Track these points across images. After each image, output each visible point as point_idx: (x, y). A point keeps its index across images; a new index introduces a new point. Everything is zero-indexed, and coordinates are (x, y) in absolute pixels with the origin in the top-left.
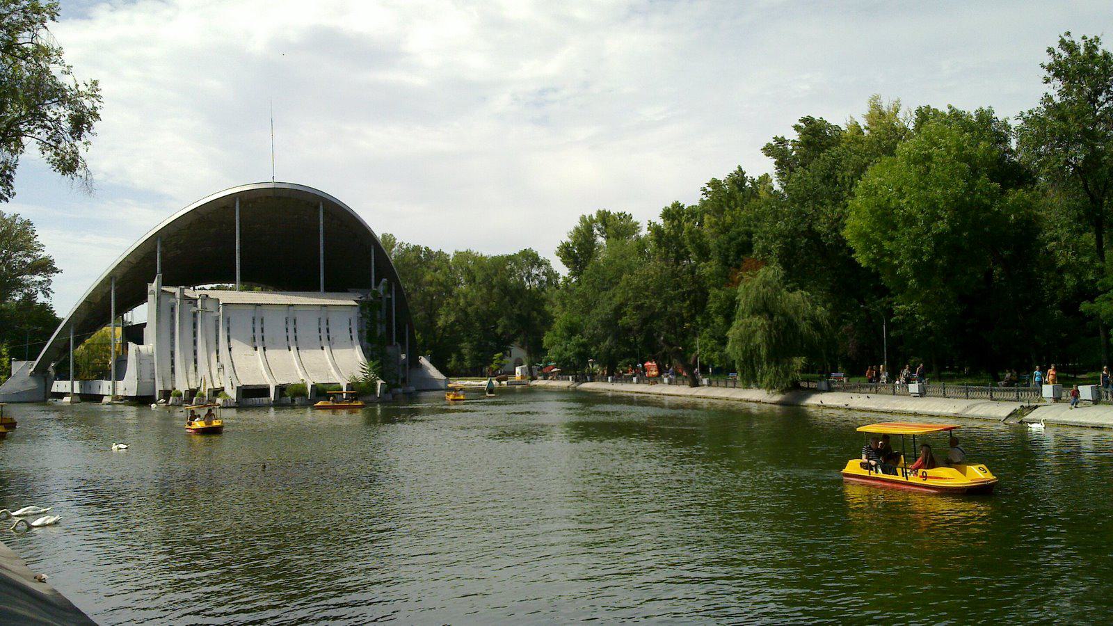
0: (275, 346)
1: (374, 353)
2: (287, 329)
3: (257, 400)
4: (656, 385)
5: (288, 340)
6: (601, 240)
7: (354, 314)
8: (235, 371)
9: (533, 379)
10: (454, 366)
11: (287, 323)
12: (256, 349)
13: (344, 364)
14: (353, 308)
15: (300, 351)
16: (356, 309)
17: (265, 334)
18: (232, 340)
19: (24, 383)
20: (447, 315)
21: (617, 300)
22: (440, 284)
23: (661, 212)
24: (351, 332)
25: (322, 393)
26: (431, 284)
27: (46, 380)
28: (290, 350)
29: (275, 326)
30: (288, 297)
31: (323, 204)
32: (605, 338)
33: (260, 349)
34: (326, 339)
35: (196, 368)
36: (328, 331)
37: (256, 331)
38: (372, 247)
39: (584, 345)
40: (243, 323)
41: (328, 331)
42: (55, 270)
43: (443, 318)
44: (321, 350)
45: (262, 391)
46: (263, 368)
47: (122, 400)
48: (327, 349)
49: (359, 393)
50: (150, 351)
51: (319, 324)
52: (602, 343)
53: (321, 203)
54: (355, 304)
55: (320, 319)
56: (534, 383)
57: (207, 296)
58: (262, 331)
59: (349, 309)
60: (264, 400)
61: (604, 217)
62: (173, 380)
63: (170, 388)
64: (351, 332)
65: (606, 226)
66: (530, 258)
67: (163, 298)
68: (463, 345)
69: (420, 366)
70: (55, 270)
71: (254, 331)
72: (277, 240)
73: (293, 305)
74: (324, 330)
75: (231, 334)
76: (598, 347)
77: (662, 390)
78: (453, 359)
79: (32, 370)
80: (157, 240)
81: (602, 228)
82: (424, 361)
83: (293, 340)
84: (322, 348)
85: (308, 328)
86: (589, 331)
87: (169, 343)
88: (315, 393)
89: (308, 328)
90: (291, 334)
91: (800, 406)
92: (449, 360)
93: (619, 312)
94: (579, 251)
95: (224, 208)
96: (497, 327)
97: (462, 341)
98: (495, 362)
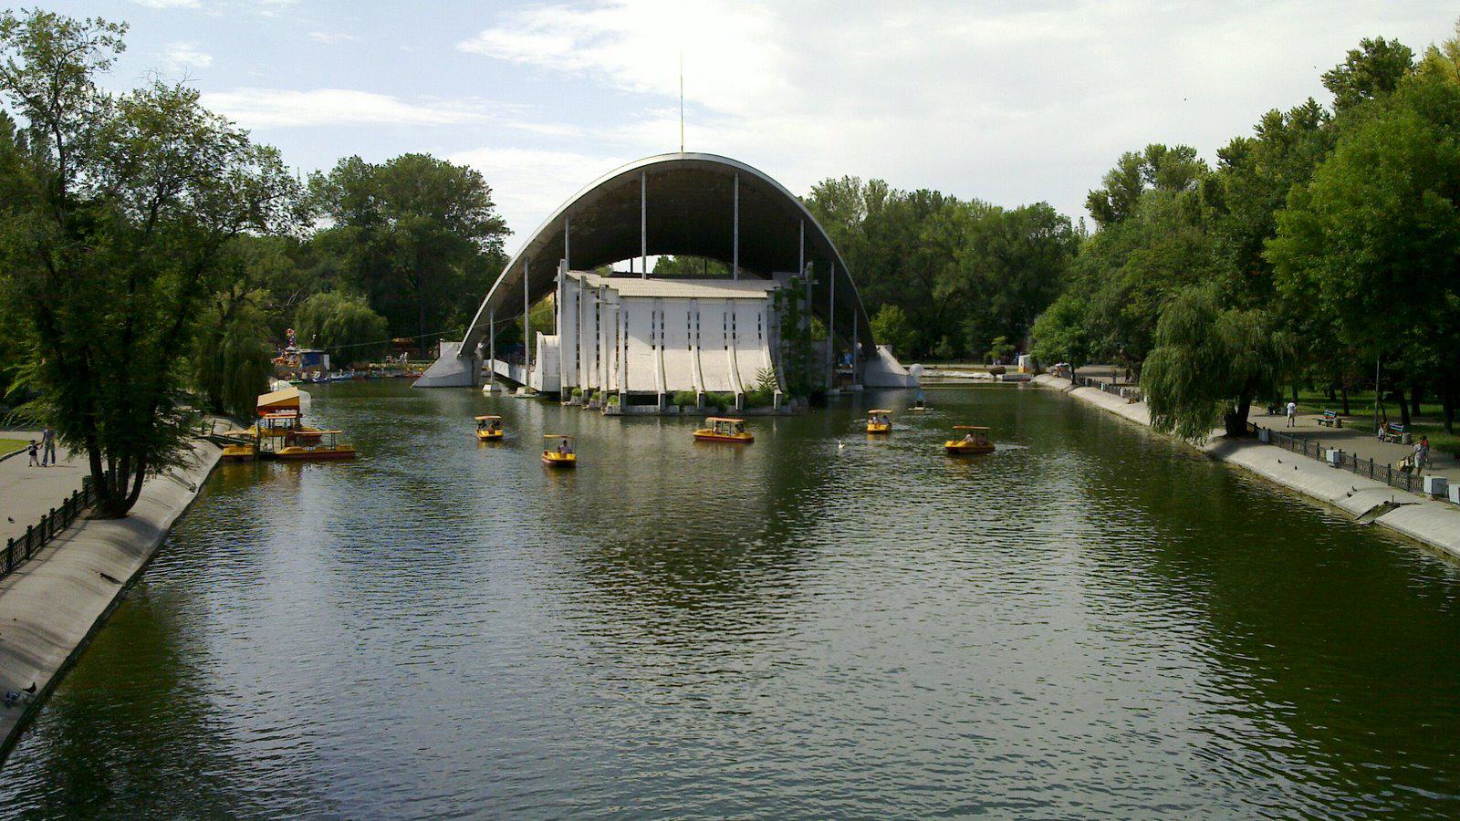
0: (675, 346)
1: (792, 352)
2: (689, 325)
3: (643, 408)
4: (1136, 404)
5: (689, 338)
6: (1149, 186)
7: (762, 308)
8: (626, 374)
9: (1039, 372)
10: (943, 352)
11: (689, 318)
12: (654, 348)
13: (743, 366)
14: (764, 301)
15: (701, 351)
16: (766, 302)
17: (665, 331)
18: (629, 337)
19: (452, 366)
20: (946, 284)
21: (1126, 282)
22: (939, 245)
23: (1085, 200)
24: (760, 329)
25: (714, 404)
26: (928, 244)
27: (473, 363)
28: (690, 349)
29: (676, 322)
30: (695, 286)
31: (739, 176)
32: (1108, 333)
33: (658, 348)
34: (731, 337)
35: (598, 365)
36: (734, 328)
37: (656, 328)
38: (802, 222)
39: (1082, 339)
40: (641, 318)
41: (734, 328)
42: (507, 231)
43: (939, 287)
44: (724, 351)
45: (649, 398)
46: (656, 371)
47: (533, 394)
48: (730, 349)
49: (751, 406)
50: (556, 344)
51: (725, 320)
52: (1105, 337)
53: (737, 175)
54: (765, 295)
55: (725, 314)
56: (1040, 379)
57: (607, 286)
58: (662, 328)
59: (758, 302)
60: (651, 408)
61: (1156, 154)
62: (578, 376)
63: (574, 385)
64: (760, 329)
65: (1158, 167)
66: (1042, 216)
67: (568, 285)
68: (966, 322)
69: (877, 358)
70: (507, 231)
71: (653, 327)
72: (693, 214)
73: (695, 298)
74: (729, 327)
75: (629, 331)
76: (1099, 342)
77: (1132, 413)
78: (943, 343)
79: (459, 352)
80: (565, 217)
81: (1152, 171)
82: (884, 351)
83: (695, 339)
84: (726, 348)
85: (712, 323)
86: (1089, 321)
87: (574, 338)
88: (703, 402)
89: (712, 323)
90: (693, 331)
91: (1222, 461)
92: (937, 343)
93: (1125, 297)
94: (1115, 204)
95: (631, 182)
96: (991, 304)
97: (965, 317)
98: (994, 348)
